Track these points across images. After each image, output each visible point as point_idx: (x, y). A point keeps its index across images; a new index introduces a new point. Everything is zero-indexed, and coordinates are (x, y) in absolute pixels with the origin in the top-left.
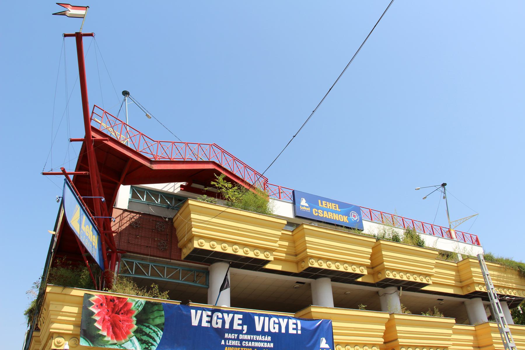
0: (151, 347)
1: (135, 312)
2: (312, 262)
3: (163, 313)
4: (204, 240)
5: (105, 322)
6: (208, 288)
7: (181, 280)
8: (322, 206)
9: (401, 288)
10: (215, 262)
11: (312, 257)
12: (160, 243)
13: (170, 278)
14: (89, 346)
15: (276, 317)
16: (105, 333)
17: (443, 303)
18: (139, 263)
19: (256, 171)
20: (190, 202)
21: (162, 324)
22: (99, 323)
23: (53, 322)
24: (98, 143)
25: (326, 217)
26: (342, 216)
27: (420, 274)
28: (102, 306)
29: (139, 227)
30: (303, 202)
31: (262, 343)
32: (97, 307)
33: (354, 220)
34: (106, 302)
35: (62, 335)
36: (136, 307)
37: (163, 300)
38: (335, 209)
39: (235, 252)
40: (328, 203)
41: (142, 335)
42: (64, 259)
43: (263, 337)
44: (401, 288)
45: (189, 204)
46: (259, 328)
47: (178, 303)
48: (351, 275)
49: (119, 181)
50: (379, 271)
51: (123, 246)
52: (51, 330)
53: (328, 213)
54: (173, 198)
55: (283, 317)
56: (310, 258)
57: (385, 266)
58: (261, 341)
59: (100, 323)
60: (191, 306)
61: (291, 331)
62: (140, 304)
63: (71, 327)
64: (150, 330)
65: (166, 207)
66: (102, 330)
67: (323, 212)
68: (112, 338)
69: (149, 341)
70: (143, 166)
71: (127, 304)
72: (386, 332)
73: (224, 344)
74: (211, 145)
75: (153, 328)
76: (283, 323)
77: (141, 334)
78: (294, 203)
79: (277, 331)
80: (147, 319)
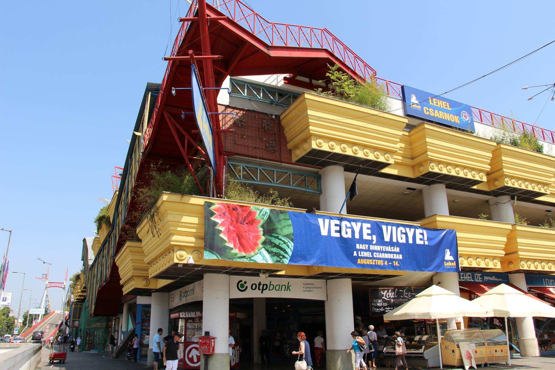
0: (283, 259)
2: (433, 166)
3: (290, 222)
5: (230, 232)
6: (320, 194)
7: (293, 185)
8: (432, 104)
9: (516, 197)
11: (432, 161)
12: (269, 144)
13: (280, 183)
14: (217, 259)
15: (403, 227)
16: (231, 245)
17: (551, 214)
18: (247, 167)
19: (365, 62)
20: (307, 96)
21: (292, 234)
23: (172, 234)
24: (214, 22)
25: (437, 116)
26: (453, 116)
27: (538, 183)
28: (225, 215)
29: (245, 126)
30: (414, 99)
31: (391, 254)
32: (220, 216)
33: (465, 121)
34: (228, 211)
36: (261, 215)
37: (286, 208)
38: (446, 108)
39: (355, 154)
40: (438, 101)
41: (271, 246)
42: (159, 164)
43: (392, 248)
44: (516, 197)
45: (306, 98)
46: (387, 239)
47: (303, 211)
48: (471, 181)
49: (227, 72)
50: (495, 178)
52: (172, 243)
53: (439, 112)
54: (275, 93)
55: (410, 227)
56: (430, 162)
57: (505, 173)
58: (391, 253)
60: (317, 214)
61: (418, 242)
62: (265, 212)
63: (193, 239)
64: (280, 241)
65: (269, 103)
67: (434, 110)
68: (240, 250)
69: (279, 253)
70: (259, 51)
71: (251, 213)
72: (507, 244)
73: (356, 255)
74: (323, 30)
76: (410, 234)
77: (270, 246)
78: (404, 100)
79: (405, 242)
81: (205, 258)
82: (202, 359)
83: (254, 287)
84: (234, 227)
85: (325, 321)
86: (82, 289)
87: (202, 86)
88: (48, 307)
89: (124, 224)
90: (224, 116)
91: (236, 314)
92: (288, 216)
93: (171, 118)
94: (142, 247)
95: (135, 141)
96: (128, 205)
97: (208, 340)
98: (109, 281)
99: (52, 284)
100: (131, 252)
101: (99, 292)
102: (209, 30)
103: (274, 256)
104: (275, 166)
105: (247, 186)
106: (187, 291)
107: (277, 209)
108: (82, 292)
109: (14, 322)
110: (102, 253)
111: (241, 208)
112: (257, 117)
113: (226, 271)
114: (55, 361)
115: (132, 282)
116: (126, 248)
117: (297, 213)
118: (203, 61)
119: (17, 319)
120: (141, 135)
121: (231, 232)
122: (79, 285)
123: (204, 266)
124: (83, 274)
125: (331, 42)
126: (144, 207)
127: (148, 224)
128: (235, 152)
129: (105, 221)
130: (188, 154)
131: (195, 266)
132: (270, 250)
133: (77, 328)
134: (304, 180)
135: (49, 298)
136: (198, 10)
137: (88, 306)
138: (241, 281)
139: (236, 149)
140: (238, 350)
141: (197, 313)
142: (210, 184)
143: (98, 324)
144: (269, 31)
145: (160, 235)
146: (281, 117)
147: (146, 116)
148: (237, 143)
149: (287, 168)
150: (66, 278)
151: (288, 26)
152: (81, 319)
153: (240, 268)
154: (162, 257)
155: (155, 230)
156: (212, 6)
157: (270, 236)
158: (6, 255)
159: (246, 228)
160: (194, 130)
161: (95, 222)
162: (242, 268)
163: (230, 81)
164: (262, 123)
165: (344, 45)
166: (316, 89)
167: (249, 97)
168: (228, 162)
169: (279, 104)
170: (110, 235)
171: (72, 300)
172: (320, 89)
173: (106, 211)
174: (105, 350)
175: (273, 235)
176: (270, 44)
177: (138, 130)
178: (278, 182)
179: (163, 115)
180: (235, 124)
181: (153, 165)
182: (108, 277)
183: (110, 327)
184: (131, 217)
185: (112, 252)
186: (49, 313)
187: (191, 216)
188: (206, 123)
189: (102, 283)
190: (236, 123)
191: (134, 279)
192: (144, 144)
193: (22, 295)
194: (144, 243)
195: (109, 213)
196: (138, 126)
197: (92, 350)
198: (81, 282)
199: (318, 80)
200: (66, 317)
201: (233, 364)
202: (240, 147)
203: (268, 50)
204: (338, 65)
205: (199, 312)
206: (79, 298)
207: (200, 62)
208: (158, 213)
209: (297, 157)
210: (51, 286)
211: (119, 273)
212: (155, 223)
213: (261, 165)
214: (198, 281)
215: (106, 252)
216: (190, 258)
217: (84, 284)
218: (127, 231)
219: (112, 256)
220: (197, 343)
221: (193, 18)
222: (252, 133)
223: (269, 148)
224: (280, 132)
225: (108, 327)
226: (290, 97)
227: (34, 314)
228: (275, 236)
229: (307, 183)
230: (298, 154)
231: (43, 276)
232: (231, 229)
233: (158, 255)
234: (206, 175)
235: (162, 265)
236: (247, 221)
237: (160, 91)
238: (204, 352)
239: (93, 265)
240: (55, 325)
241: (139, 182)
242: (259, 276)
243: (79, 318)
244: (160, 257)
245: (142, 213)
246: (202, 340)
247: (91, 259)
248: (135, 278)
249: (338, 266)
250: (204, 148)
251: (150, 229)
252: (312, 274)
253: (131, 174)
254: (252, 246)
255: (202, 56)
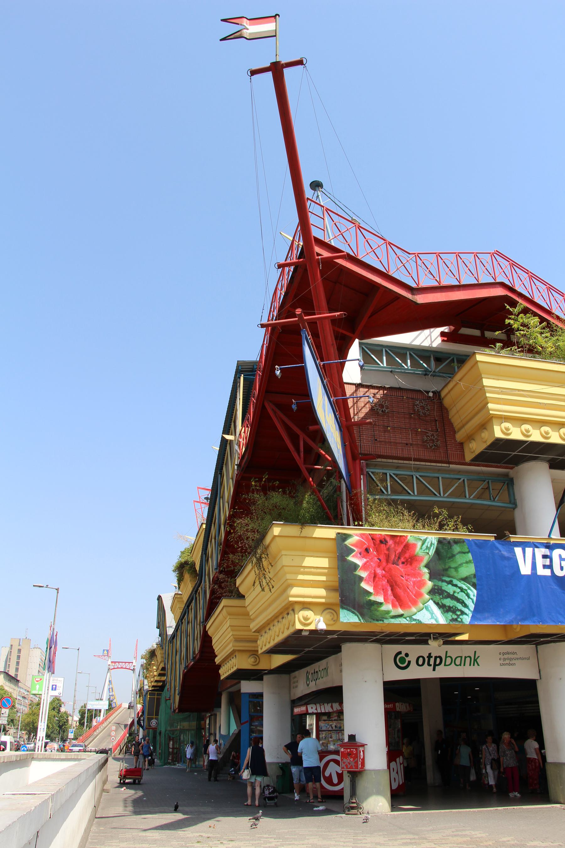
0: (461, 617)
1: (423, 558)
3: (470, 557)
4: (508, 422)
5: (377, 579)
6: (514, 509)
7: (470, 496)
10: (523, 462)
13: (450, 496)
18: (397, 475)
20: (479, 358)
22: (368, 583)
23: (291, 586)
24: (328, 262)
28: (368, 553)
32: (361, 555)
34: (373, 545)
35: (308, 606)
37: (463, 534)
42: (264, 480)
47: (490, 537)
49: (354, 333)
51: (367, 448)
52: (291, 599)
54: (430, 357)
59: (369, 583)
62: (429, 544)
63: (322, 592)
65: (422, 374)
66: (374, 594)
68: (394, 606)
69: (455, 607)
70: (399, 298)
71: (408, 547)
75: (460, 584)
77: (441, 596)
80: (446, 570)
81: (341, 620)
82: (347, 779)
83: (421, 661)
84: (384, 569)
85: (539, 712)
86: (159, 671)
87: (319, 360)
88: (112, 697)
89: (216, 572)
90: (355, 400)
91: (394, 706)
92: (467, 547)
93: (277, 410)
94: (246, 607)
95: (226, 448)
96: (221, 544)
97: (353, 749)
98: (199, 659)
99: (117, 665)
100: (229, 614)
101: (185, 675)
102: (322, 276)
103: (447, 611)
104: (439, 470)
105: (399, 504)
106: (317, 672)
107: (449, 537)
108: (160, 675)
109: (67, 720)
110: (186, 617)
111: (393, 540)
112: (405, 397)
113: (375, 638)
114: (127, 781)
115: (233, 660)
116: (222, 609)
117: (481, 541)
118: (318, 322)
119: (73, 716)
120: (234, 439)
121: (379, 578)
122: (155, 666)
123: (341, 632)
124: (160, 649)
125: (508, 271)
126: (246, 547)
127: (253, 572)
128: (377, 453)
129: (188, 568)
130: (305, 462)
131: (327, 632)
132: (441, 602)
133: (155, 730)
134: (487, 489)
135: (114, 685)
136: (302, 248)
137: (170, 697)
138: (400, 653)
139: (378, 448)
140: (401, 764)
141: (334, 705)
142: (342, 506)
143: (186, 724)
144: (411, 266)
145: (273, 587)
146: (443, 394)
147: (238, 411)
148: (378, 440)
149: (459, 472)
150: (136, 655)
151: (440, 254)
152: (159, 717)
153: (398, 633)
154: (276, 621)
155: (264, 580)
156: (323, 240)
157: (439, 581)
158: (53, 624)
159: (402, 570)
160: (311, 425)
161: (174, 571)
162: (400, 633)
163: (360, 346)
164: (414, 405)
165: (529, 273)
166: (492, 346)
167: (390, 368)
168: (368, 470)
169: (437, 374)
170: (197, 590)
171: (146, 687)
172: (498, 345)
173: (189, 554)
174: (197, 763)
175: (444, 578)
176: (414, 285)
177: (229, 432)
178: (446, 495)
179: (264, 407)
180: (373, 411)
181: (255, 482)
182: (196, 653)
183: (203, 729)
184: (228, 562)
185: (201, 614)
186: (114, 707)
187: (317, 557)
188: (330, 414)
189: (189, 662)
190: (375, 409)
191: (236, 656)
192: (239, 451)
193: (76, 680)
194: (248, 601)
195: (193, 557)
196: (228, 427)
197: (178, 763)
198: (157, 660)
199: (495, 331)
200: (138, 713)
201: (395, 786)
202: (383, 445)
203: (413, 294)
204: (523, 304)
205: (337, 704)
206: (155, 684)
207: (313, 325)
208: (267, 555)
209: (472, 452)
210: (116, 667)
211: (212, 646)
212: (264, 569)
213: (417, 469)
214: (333, 656)
215: (192, 615)
216: (319, 621)
217: (161, 664)
218: (223, 582)
219: (202, 620)
220: (336, 752)
221: (297, 260)
222: (399, 422)
223: (428, 443)
224: (443, 417)
225: (200, 728)
226: (453, 361)
227: (93, 710)
228: (447, 580)
229: (491, 491)
230: (474, 448)
231: (103, 652)
232: (378, 574)
233: (271, 618)
234: (335, 491)
235: (277, 633)
236: (402, 559)
237: (258, 372)
238: (349, 767)
239: (174, 636)
240: (123, 726)
241: (236, 509)
242: (428, 644)
243: (157, 714)
244: (273, 620)
245: (242, 556)
246: (344, 748)
247: (171, 625)
248: (237, 654)
249: (553, 624)
250: (329, 451)
251: (257, 579)
252: (513, 636)
253: (222, 497)
254: (413, 599)
255: (315, 315)
